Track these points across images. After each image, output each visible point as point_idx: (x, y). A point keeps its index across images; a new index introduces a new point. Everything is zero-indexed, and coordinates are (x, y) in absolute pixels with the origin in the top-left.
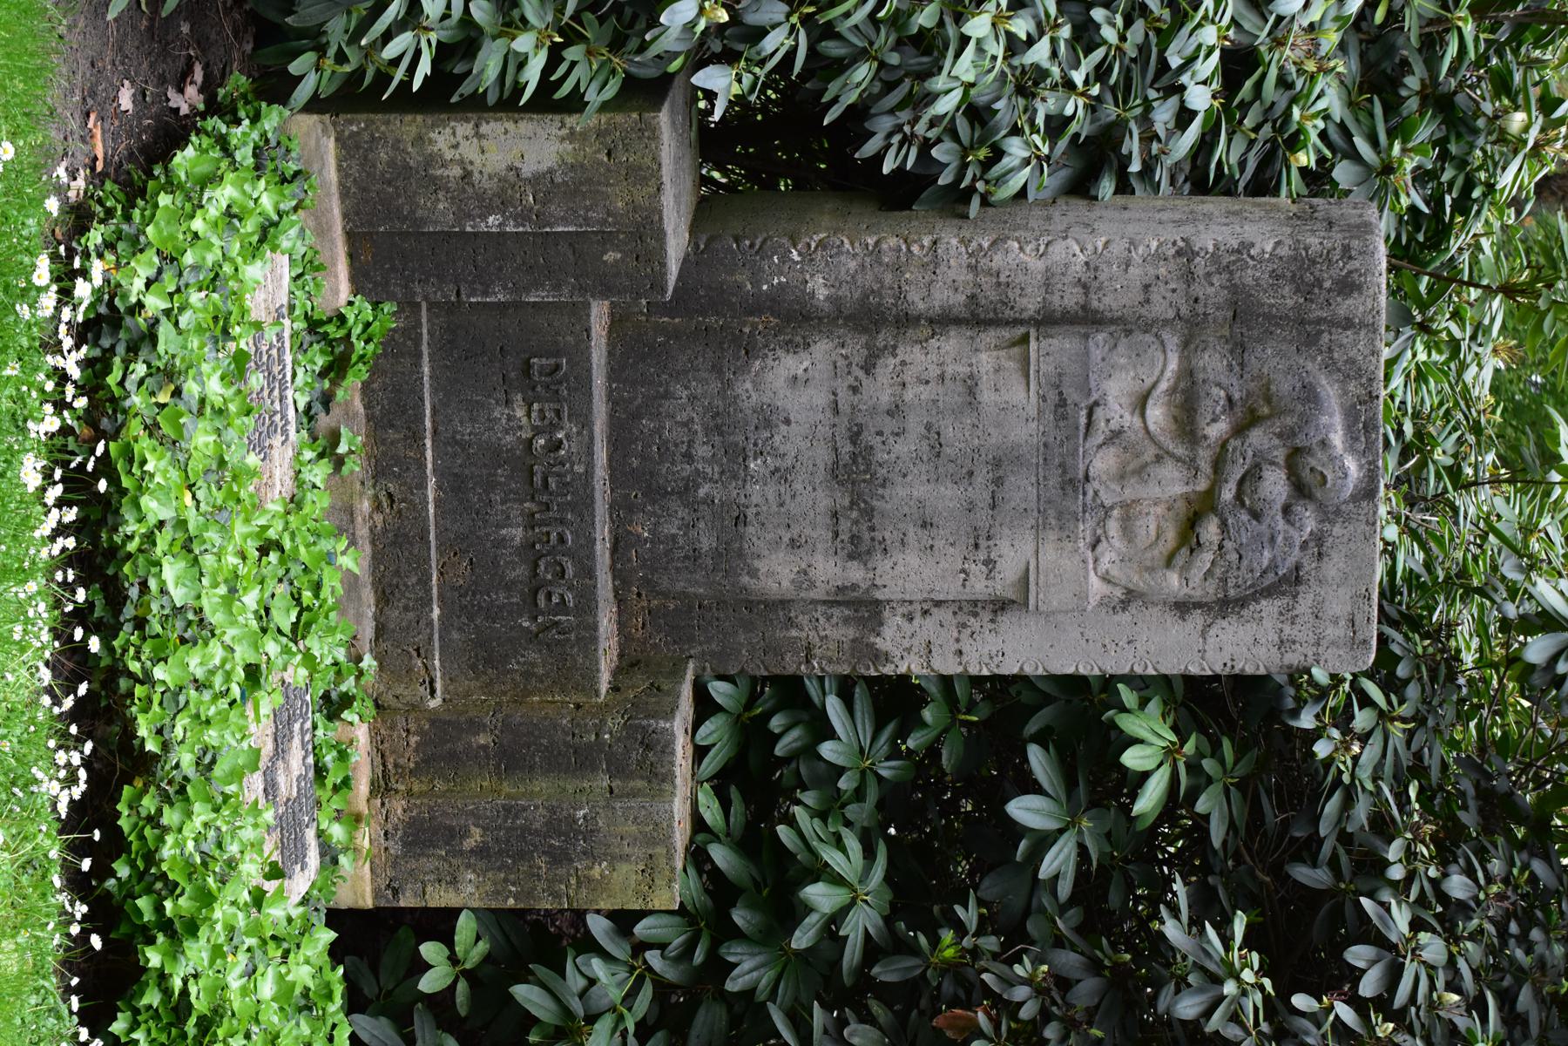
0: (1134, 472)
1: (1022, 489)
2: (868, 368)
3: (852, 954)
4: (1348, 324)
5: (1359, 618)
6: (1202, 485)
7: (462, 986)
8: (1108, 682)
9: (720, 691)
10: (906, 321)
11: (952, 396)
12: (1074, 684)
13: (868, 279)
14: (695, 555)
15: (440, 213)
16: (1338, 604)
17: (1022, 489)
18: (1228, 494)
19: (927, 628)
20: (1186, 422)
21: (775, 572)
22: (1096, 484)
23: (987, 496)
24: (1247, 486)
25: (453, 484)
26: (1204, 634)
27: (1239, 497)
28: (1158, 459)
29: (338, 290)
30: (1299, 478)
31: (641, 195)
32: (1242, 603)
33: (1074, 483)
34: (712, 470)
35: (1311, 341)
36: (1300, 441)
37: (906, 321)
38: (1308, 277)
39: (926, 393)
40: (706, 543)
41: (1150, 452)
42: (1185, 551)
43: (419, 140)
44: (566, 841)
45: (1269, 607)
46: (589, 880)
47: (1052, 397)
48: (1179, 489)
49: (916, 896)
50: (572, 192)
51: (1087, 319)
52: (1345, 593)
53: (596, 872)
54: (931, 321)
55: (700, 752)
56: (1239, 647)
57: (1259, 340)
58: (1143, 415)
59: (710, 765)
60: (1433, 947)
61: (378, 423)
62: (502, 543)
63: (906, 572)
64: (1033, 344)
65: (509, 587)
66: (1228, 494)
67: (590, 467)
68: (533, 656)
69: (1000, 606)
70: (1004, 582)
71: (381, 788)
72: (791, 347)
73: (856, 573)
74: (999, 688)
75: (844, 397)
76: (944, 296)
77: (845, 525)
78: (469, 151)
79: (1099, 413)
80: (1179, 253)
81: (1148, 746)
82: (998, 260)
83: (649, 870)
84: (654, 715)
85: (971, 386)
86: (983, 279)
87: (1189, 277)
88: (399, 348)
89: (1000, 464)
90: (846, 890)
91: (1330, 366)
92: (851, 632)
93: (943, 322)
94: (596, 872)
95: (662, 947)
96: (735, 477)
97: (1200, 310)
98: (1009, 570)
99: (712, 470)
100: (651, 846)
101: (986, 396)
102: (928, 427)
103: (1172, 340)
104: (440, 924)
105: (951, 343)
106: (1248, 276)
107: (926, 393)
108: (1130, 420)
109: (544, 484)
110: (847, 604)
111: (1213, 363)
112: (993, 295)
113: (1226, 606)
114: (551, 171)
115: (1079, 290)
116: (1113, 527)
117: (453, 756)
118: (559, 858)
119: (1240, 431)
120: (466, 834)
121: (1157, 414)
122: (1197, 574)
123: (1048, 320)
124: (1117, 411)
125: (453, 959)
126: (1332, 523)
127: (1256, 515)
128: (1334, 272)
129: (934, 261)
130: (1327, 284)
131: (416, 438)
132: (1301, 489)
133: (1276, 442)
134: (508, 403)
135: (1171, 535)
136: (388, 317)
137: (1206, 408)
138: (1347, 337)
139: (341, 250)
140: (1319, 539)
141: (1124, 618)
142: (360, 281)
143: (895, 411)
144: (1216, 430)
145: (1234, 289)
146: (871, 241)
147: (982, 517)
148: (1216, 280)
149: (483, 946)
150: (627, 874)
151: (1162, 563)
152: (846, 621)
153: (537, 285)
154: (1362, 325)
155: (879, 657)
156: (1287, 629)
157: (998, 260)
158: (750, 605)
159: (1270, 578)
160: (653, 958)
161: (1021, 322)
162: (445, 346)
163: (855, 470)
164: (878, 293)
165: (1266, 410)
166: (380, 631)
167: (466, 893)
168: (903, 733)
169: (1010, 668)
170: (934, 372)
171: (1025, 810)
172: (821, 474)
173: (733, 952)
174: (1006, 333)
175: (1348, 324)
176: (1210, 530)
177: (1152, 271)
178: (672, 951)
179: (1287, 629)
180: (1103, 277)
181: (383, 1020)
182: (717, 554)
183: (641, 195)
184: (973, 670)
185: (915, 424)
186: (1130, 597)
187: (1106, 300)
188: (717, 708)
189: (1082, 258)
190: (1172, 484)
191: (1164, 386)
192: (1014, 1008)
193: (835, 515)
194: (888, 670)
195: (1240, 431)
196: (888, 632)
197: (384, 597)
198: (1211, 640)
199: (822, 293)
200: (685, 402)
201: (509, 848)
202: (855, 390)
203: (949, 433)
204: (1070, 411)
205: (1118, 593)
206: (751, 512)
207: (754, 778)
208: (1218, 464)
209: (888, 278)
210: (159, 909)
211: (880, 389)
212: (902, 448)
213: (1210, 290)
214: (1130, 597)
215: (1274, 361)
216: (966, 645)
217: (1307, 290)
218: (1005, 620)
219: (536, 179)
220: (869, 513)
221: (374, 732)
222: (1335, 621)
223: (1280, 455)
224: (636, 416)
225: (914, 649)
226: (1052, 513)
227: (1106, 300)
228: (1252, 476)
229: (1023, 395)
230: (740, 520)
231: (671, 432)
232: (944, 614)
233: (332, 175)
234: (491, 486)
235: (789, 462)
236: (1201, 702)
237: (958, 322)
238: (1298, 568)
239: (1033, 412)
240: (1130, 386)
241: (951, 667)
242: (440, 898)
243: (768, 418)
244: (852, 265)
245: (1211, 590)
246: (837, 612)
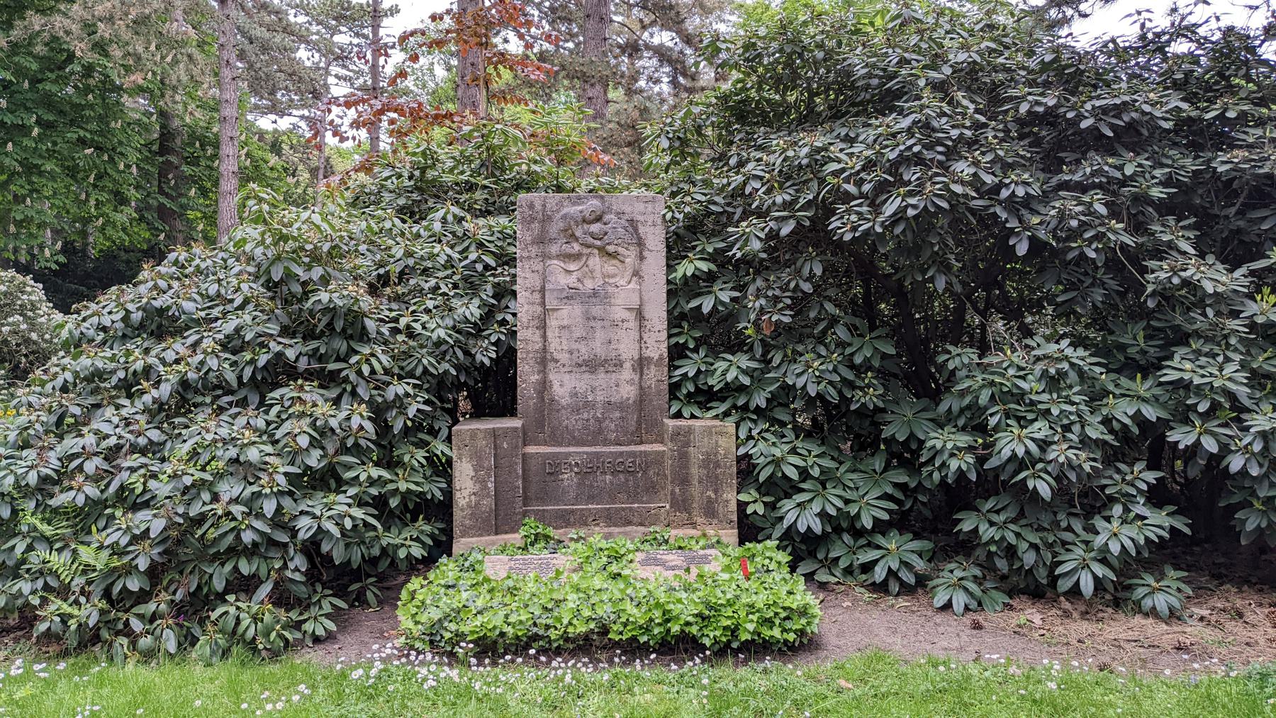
1: (597, 310)
2: (557, 361)
3: (754, 365)
6: (596, 251)
7: (765, 499)
8: (669, 282)
9: (674, 410)
10: (545, 349)
11: (565, 333)
12: (671, 294)
15: (488, 503)
17: (597, 310)
18: (598, 243)
20: (576, 257)
21: (628, 392)
25: (591, 499)
29: (516, 538)
31: (480, 435)
32: (640, 238)
33: (595, 293)
34: (592, 413)
35: (550, 218)
36: (579, 219)
39: (565, 342)
40: (617, 414)
43: (462, 510)
44: (711, 462)
45: (641, 230)
48: (597, 258)
49: (738, 345)
50: (480, 458)
51: (543, 291)
52: (636, 205)
55: (693, 416)
59: (697, 413)
60: (750, 166)
61: (568, 524)
63: (627, 348)
65: (627, 480)
67: (587, 453)
70: (631, 316)
71: (694, 525)
72: (551, 387)
73: (628, 365)
76: (537, 337)
78: (466, 493)
83: (721, 434)
87: (529, 258)
88: (542, 517)
89: (589, 318)
90: (730, 368)
91: (558, 211)
93: (544, 337)
95: (750, 430)
98: (626, 315)
99: (592, 413)
100: (715, 434)
101: (565, 323)
103: (549, 262)
104: (742, 506)
105: (549, 334)
107: (565, 342)
108: (575, 275)
109: (589, 469)
111: (554, 249)
113: (640, 243)
116: (611, 281)
118: (717, 465)
119: (577, 239)
120: (709, 497)
121: (572, 267)
122: (626, 253)
124: (571, 280)
125: (755, 502)
127: (606, 234)
129: (526, 341)
131: (573, 511)
132: (598, 219)
135: (615, 262)
136: (530, 521)
139: (499, 537)
142: (514, 530)
143: (571, 353)
145: (533, 243)
147: (607, 323)
149: (752, 491)
150: (723, 442)
155: (661, 358)
158: (641, 401)
159: (630, 229)
160: (754, 433)
162: (543, 501)
163: (591, 365)
166: (641, 524)
167: (731, 497)
168: (688, 349)
171: (706, 309)
173: (752, 406)
175: (544, 206)
176: (611, 248)
178: (752, 426)
182: (622, 411)
183: (480, 435)
188: (680, 411)
190: (595, 261)
192: (762, 308)
194: (666, 355)
195: (577, 239)
197: (629, 523)
199: (537, 377)
201: (714, 481)
203: (578, 335)
204: (570, 295)
207: (704, 397)
208: (588, 246)
210: (660, 624)
211: (564, 357)
212: (583, 350)
214: (636, 273)
215: (554, 228)
217: (533, 219)
219: (476, 471)
220: (606, 361)
221: (675, 528)
223: (586, 226)
224: (574, 438)
225: (657, 346)
228: (592, 235)
231: (580, 425)
232: (645, 337)
233: (474, 539)
234: (592, 486)
236: (677, 247)
241: (665, 334)
242: (733, 506)
243: (574, 394)
246: (646, 372)
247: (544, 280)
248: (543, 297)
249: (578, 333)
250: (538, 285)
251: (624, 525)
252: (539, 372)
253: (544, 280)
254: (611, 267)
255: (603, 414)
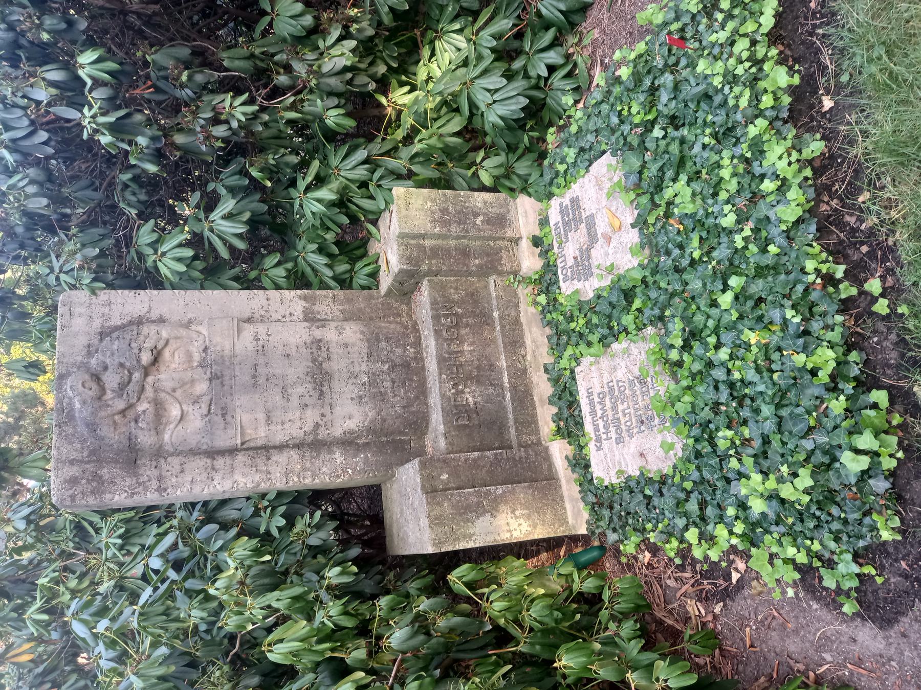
0: (186, 384)
2: (317, 425)
4: (72, 462)
5: (68, 317)
6: (150, 379)
10: (299, 446)
11: (278, 415)
13: (318, 463)
14: (387, 339)
16: (79, 323)
18: (137, 376)
19: (283, 310)
20: (159, 406)
21: (352, 332)
22: (206, 377)
23: (260, 370)
24: (126, 379)
26: (150, 308)
27: (131, 374)
28: (174, 390)
30: (99, 384)
31: (437, 511)
32: (131, 323)
36: (97, 404)
37: (299, 446)
38: (94, 484)
39: (290, 416)
41: (178, 394)
42: (159, 347)
45: (116, 321)
46: (432, 201)
47: (229, 418)
48: (162, 376)
50: (468, 509)
51: (213, 453)
53: (429, 204)
54: (288, 446)
56: (129, 303)
57: (122, 451)
58: (182, 411)
62: (472, 344)
63: (296, 334)
64: (239, 442)
65: (467, 325)
66: (137, 376)
68: (455, 297)
69: (249, 320)
70: (249, 330)
72: (351, 432)
74: (248, 284)
75: (327, 410)
76: (281, 458)
77: (324, 354)
79: (205, 412)
80: (165, 490)
81: (171, 257)
82: (257, 477)
84: (407, 271)
85: (269, 420)
86: (264, 468)
87: (160, 478)
92: (316, 308)
93: (281, 447)
94: (429, 204)
96: (373, 374)
97: (154, 463)
101: (261, 416)
102: (288, 400)
105: (279, 438)
106: (128, 482)
107: (290, 416)
110: (319, 320)
112: (258, 461)
113: (139, 322)
114: (478, 518)
115: (217, 467)
116: (197, 357)
117: (488, 255)
120: (482, 222)
121: (174, 412)
123: (232, 452)
126: (82, 362)
128: (80, 488)
130: (84, 481)
132: (97, 378)
133: (110, 403)
134: (475, 403)
135: (167, 354)
137: (150, 416)
138: (74, 455)
140: (89, 354)
141: (190, 315)
144: (142, 406)
145: (136, 475)
146: (317, 481)
147: (261, 360)
148: (145, 478)
151: (171, 341)
152: (319, 313)
153: (475, 460)
154: (64, 462)
155: (305, 298)
156: (107, 311)
157: (257, 477)
159: (114, 335)
161: (247, 449)
163: (320, 379)
164: (313, 457)
165: (116, 417)
166: (517, 306)
169: (246, 293)
170: (286, 426)
172: (336, 376)
174: (252, 444)
176: (146, 358)
177: (179, 479)
179: (107, 311)
180: (205, 475)
181: (773, 20)
182: (378, 340)
183: (437, 511)
184: (261, 292)
185: (295, 401)
186: (188, 324)
187: (202, 463)
189: (215, 482)
190: (165, 377)
191: (172, 426)
193: (329, 359)
194: (299, 292)
196: (300, 308)
198: (146, 305)
199: (337, 455)
200: (396, 406)
202: (323, 415)
203: (278, 398)
204: (220, 411)
205: (193, 327)
206: (365, 359)
208: (143, 389)
209: (308, 465)
211: (312, 416)
212: (300, 390)
213: (149, 473)
214: (188, 324)
216: (265, 302)
217: (97, 477)
218: (247, 314)
219: (485, 512)
220: (314, 360)
222: (80, 315)
223: (109, 395)
224: (417, 398)
226: (227, 363)
227: (202, 463)
229: (244, 418)
230: (370, 355)
235: (351, 381)
237: (275, 447)
238: (101, 340)
239: (238, 410)
240: (186, 423)
244: (324, 469)
245: (145, 330)
246: (323, 316)
247: (194, 452)
248: (222, 452)
249: (277, 398)
250: (202, 462)
251: (521, 325)
252: (331, 452)
253: (194, 452)
254: (173, 360)
255: (383, 362)
